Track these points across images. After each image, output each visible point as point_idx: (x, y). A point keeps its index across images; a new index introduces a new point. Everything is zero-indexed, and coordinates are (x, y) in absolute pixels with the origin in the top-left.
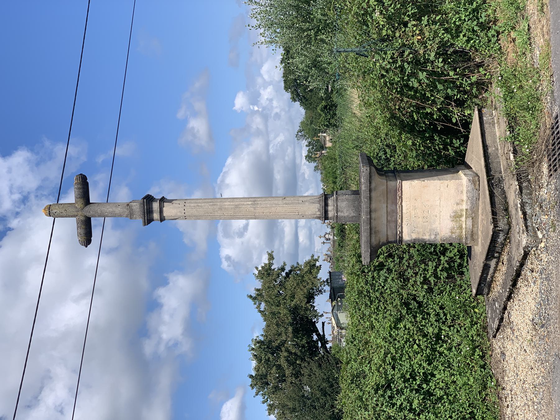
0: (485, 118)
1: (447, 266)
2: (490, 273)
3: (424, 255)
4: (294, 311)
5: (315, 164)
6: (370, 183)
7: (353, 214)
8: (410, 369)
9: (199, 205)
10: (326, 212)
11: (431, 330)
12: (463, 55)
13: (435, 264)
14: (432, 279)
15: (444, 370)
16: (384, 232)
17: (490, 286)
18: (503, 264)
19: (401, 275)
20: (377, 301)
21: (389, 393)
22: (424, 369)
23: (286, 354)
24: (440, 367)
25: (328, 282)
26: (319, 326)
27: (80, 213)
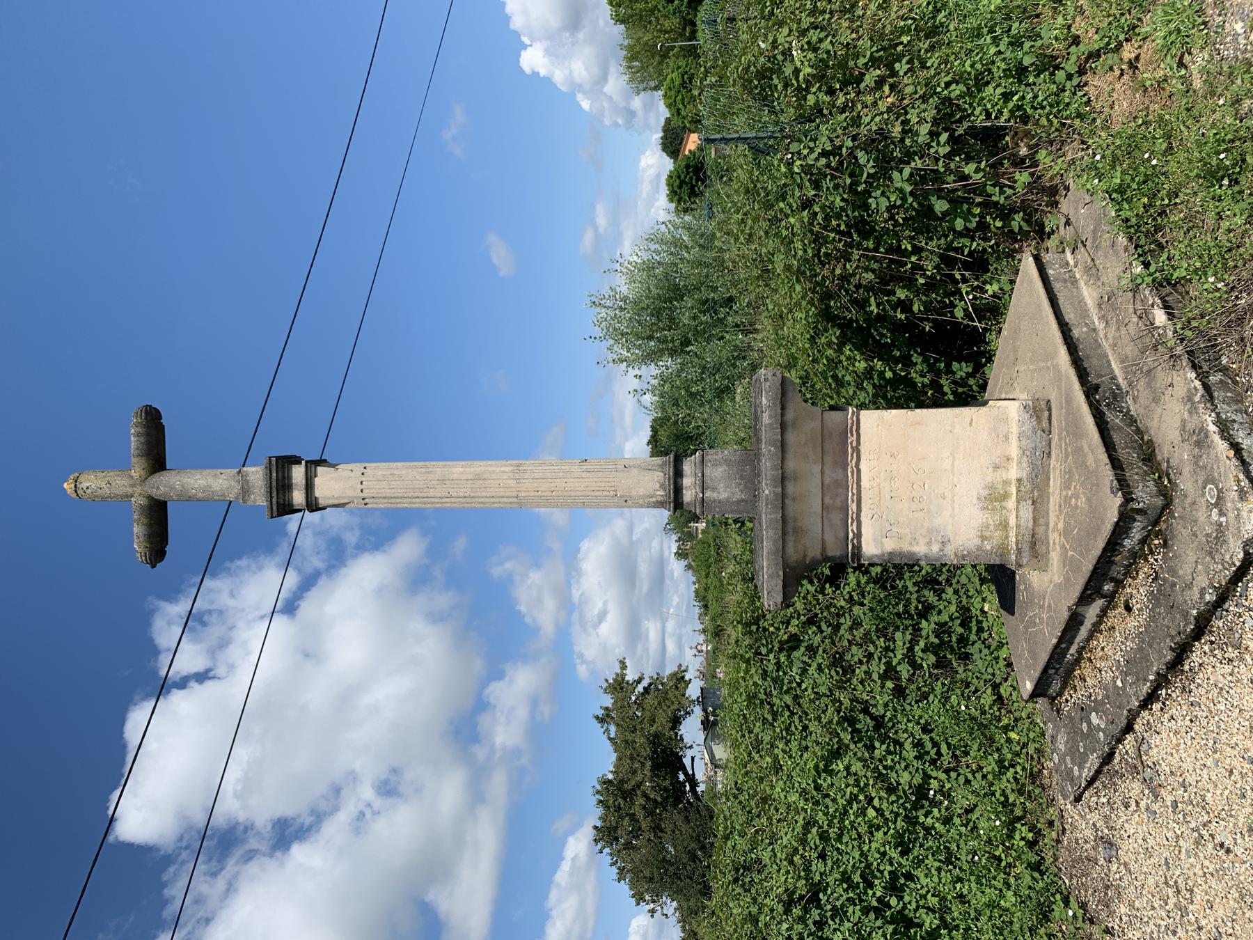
0: (1050, 272)
1: (937, 641)
2: (1077, 641)
3: (883, 619)
6: (783, 408)
7: (739, 495)
8: (861, 862)
9: (396, 472)
10: (678, 490)
11: (905, 777)
12: (991, 138)
13: (909, 637)
14: (905, 670)
15: (939, 870)
16: (817, 538)
17: (1069, 673)
18: (1128, 609)
19: (837, 660)
20: (787, 714)
21: (815, 914)
22: (891, 864)
23: (642, 801)
24: (930, 861)
26: (687, 762)
27: (138, 490)
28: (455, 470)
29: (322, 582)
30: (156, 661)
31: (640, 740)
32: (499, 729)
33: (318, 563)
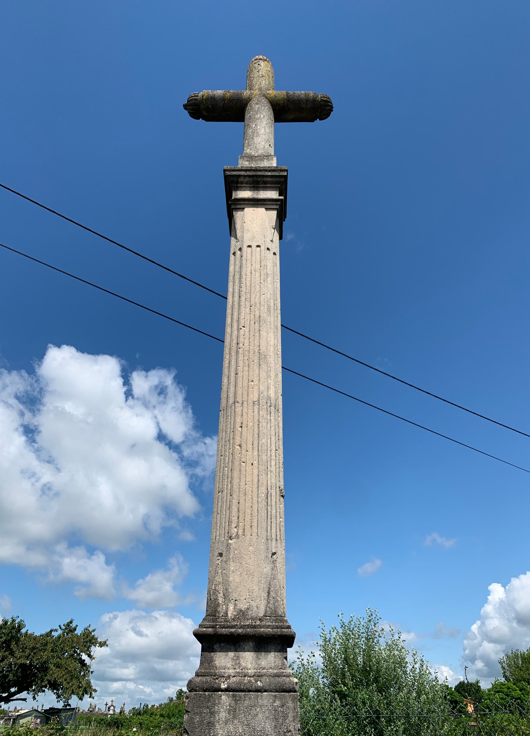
4: (44, 668)
5: (175, 699)
9: (269, 279)
25: (66, 706)
27: (257, 92)
28: (272, 335)
29: (175, 455)
30: (141, 370)
31: (45, 656)
32: (74, 560)
33: (186, 452)
